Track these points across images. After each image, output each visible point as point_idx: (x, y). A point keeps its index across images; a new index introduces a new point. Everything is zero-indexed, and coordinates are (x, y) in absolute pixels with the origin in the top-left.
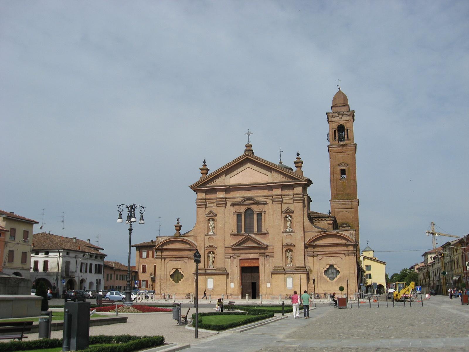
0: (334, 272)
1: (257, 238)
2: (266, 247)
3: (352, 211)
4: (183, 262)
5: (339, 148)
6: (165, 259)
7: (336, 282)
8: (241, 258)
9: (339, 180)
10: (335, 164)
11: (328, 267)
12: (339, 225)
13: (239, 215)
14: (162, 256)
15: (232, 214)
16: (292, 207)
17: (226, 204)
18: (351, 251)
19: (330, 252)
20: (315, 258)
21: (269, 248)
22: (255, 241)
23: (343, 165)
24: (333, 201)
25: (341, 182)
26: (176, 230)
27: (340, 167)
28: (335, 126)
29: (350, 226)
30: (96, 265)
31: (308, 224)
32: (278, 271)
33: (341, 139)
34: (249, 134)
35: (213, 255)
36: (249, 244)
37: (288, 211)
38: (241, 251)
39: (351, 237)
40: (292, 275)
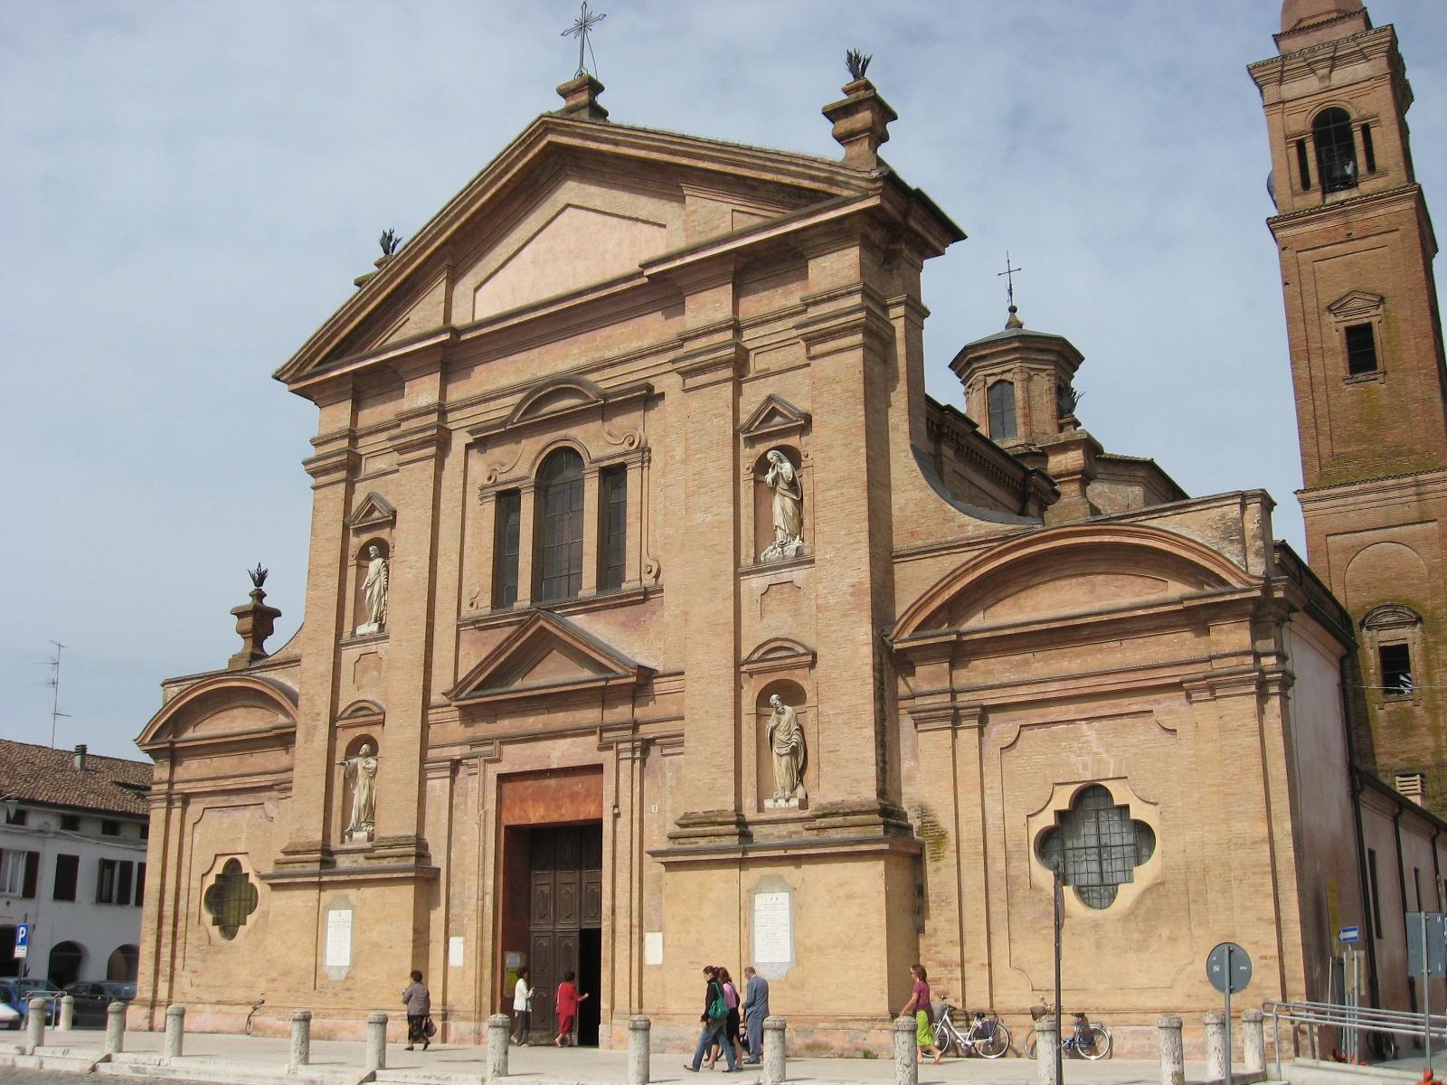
0: (1116, 840)
1: (598, 628)
2: (642, 683)
3: (1426, 538)
4: (257, 812)
5: (1329, 224)
6: (186, 799)
7: (1128, 916)
8: (504, 768)
9: (1341, 384)
10: (1310, 304)
11: (1063, 801)
12: (1356, 621)
13: (507, 501)
14: (177, 787)
15: (473, 499)
16: (797, 393)
17: (442, 442)
18: (1234, 661)
19: (1071, 684)
20: (968, 736)
21: (659, 686)
22: (581, 651)
23: (1357, 304)
24: (1315, 494)
25: (1352, 393)
26: (242, 633)
27: (1341, 318)
28: (1301, 122)
29: (1419, 619)
30: (106, 865)
31: (918, 495)
32: (703, 843)
33: (1332, 181)
34: (583, 26)
35: (372, 762)
36: (554, 673)
37: (778, 419)
38: (506, 725)
39: (1232, 553)
40: (787, 871)
